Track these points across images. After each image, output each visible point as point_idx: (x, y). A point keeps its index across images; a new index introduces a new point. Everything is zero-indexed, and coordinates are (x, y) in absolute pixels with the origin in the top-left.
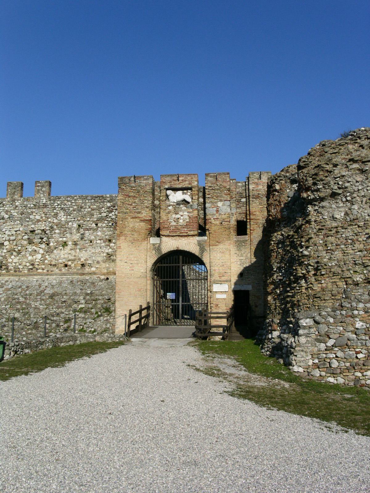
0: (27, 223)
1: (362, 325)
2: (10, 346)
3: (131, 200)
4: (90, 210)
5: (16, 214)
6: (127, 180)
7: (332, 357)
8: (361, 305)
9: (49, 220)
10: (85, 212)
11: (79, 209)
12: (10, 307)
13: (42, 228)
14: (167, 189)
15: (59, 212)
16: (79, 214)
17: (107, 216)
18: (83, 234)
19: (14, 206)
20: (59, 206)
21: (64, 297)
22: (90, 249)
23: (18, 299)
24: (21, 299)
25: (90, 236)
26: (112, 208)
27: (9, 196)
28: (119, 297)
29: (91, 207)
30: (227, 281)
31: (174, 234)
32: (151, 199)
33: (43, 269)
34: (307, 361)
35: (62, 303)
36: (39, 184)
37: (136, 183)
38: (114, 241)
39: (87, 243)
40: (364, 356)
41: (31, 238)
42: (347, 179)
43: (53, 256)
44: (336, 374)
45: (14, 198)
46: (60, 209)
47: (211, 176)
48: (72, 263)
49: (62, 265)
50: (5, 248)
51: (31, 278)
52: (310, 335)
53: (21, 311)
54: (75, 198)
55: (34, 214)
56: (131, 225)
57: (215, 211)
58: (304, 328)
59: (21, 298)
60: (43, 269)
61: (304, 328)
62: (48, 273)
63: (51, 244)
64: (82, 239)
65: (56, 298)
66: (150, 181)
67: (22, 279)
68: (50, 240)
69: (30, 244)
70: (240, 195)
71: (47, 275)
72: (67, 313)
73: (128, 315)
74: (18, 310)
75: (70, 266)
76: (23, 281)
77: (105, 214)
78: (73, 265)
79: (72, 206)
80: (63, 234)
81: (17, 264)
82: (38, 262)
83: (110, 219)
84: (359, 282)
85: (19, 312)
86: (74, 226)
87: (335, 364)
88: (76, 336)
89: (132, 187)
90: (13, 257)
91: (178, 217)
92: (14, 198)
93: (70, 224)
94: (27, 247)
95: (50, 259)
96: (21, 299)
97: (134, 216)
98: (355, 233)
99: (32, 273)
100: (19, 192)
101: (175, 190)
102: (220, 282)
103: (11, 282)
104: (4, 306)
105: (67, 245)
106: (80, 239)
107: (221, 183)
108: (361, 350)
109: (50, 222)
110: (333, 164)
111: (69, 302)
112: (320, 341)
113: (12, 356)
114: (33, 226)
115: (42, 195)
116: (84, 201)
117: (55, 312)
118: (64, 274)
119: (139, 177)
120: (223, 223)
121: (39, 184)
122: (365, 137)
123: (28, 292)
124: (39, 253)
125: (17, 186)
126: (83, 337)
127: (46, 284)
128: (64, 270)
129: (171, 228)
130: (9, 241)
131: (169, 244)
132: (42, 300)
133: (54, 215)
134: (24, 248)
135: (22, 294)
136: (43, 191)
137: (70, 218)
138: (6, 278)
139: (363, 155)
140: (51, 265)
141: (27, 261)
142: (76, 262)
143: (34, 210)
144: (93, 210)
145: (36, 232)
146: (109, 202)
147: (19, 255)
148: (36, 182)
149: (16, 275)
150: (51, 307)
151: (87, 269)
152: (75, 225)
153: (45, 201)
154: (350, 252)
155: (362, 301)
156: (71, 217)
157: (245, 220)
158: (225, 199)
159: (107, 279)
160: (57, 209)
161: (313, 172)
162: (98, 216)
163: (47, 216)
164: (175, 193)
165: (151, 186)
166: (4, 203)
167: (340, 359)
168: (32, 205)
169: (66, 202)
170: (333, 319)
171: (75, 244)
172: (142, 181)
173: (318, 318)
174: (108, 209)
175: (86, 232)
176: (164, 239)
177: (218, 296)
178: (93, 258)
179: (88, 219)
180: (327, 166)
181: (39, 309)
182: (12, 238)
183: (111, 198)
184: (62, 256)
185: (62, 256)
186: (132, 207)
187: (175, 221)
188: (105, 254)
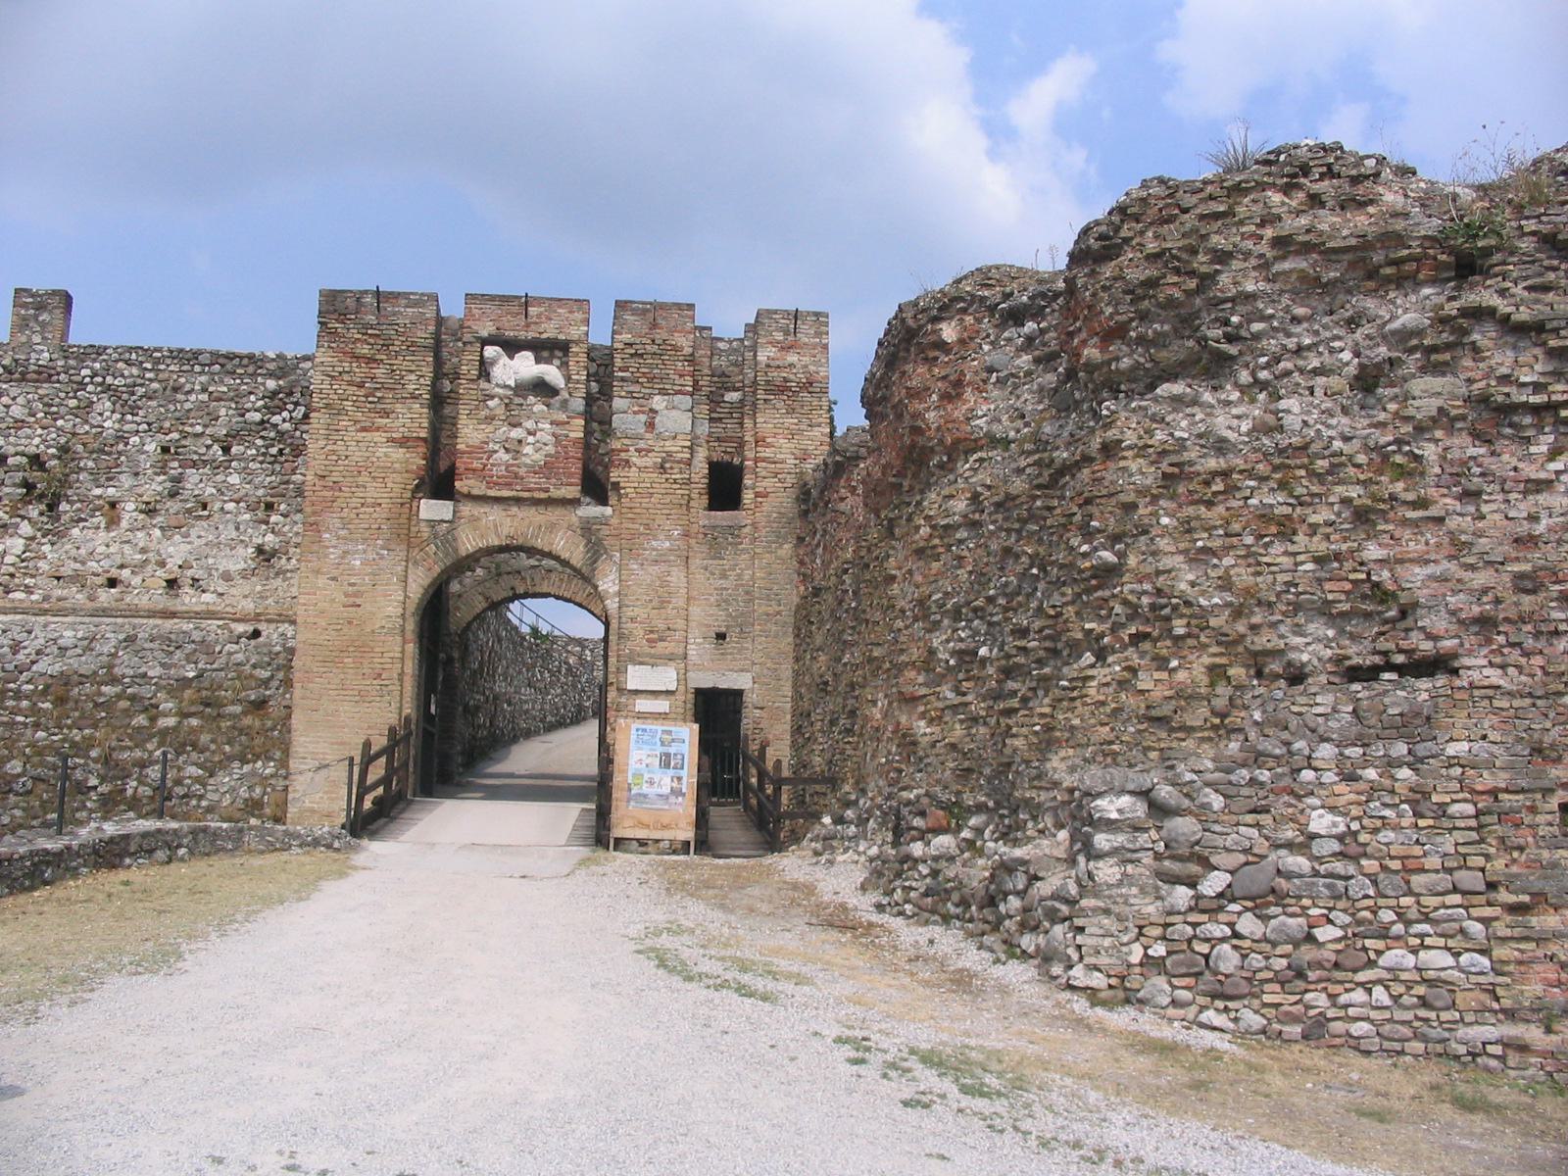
1: (1335, 825)
7: (1218, 934)
8: (1326, 751)
9: (60, 423)
11: (168, 392)
13: (32, 450)
16: (167, 411)
17: (262, 422)
20: (99, 379)
25: (201, 485)
29: (211, 389)
30: (671, 658)
32: (428, 371)
34: (1125, 949)
40: (1340, 933)
42: (1261, 306)
47: (633, 310)
52: (1138, 855)
58: (1110, 825)
61: (1110, 825)
66: (430, 313)
73: (357, 760)
77: (257, 417)
78: (136, 581)
82: (13, 565)
83: (272, 434)
84: (1307, 670)
86: (146, 448)
87: (1227, 959)
89: (368, 326)
98: (1297, 498)
101: (512, 347)
102: (652, 661)
107: (665, 336)
108: (1325, 911)
110: (1215, 251)
112: (1175, 880)
115: (37, 339)
116: (185, 368)
118: (105, 612)
120: (667, 465)
122: (1321, 170)
128: (106, 597)
131: (484, 527)
133: (78, 407)
136: (43, 325)
139: (1324, 227)
140: (58, 578)
144: (219, 399)
146: (271, 375)
151: (189, 599)
154: (1279, 560)
155: (1334, 736)
157: (736, 461)
158: (676, 388)
159: (256, 634)
160: (90, 388)
161: (1135, 275)
164: (511, 357)
165: (432, 328)
167: (1247, 944)
170: (1221, 798)
173: (1165, 792)
176: (467, 509)
178: (211, 561)
179: (199, 429)
183: (281, 364)
186: (362, 392)
187: (507, 450)
188: (251, 550)
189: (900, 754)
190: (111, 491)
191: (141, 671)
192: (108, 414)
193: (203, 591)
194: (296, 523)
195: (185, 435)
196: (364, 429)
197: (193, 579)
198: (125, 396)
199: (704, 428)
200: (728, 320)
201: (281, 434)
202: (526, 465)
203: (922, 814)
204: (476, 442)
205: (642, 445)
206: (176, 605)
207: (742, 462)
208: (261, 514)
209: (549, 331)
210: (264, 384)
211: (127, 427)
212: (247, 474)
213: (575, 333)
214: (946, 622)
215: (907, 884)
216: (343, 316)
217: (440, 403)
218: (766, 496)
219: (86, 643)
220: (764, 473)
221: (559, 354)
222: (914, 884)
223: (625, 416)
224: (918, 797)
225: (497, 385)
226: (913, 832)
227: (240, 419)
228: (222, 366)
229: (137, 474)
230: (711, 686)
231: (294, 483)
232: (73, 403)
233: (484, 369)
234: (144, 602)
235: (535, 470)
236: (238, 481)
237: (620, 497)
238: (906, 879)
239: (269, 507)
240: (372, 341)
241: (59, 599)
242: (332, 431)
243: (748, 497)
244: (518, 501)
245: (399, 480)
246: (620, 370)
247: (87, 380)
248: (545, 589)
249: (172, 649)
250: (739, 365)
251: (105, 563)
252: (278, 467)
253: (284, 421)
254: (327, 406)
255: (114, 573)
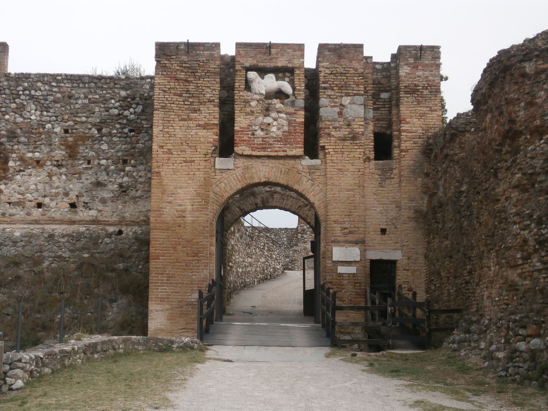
4: (86, 101)
9: (7, 117)
10: (77, 106)
14: (248, 69)
15: (25, 103)
17: (119, 114)
20: (27, 92)
25: (87, 151)
26: (129, 99)
29: (90, 96)
31: (262, 153)
38: (133, 162)
46: (28, 97)
49: (34, 204)
57: (337, 114)
70: (378, 86)
77: (116, 112)
78: (53, 204)
79: (51, 93)
83: (125, 122)
91: (269, 122)
101: (263, 72)
109: (7, 120)
116: (75, 85)
128: (37, 213)
129: (256, 142)
133: (17, 108)
137: (47, 116)
140: (9, 203)
146: (123, 88)
156: (49, 114)
157: (388, 132)
158: (355, 92)
159: (120, 232)
160: (23, 97)
162: (103, 114)
164: (263, 78)
172: (201, 52)
174: (121, 102)
177: (341, 269)
179: (84, 119)
186: (181, 99)
187: (262, 130)
188: (116, 186)
189: (508, 295)
190: (37, 154)
191: (58, 254)
192: (33, 111)
193: (90, 209)
194: (140, 171)
195: (76, 123)
196: (184, 120)
197: (84, 203)
198: (42, 101)
199: (371, 114)
200: (380, 52)
201: (129, 121)
202: (273, 137)
203: (524, 327)
204: (246, 126)
205: (337, 124)
206: (77, 218)
207: (391, 132)
208: (120, 166)
209: (281, 62)
210: (119, 93)
211: (44, 119)
212: (111, 144)
213: (296, 63)
214: (533, 225)
215: (516, 364)
216: (169, 57)
217: (227, 106)
218: (407, 152)
219: (26, 239)
220: (405, 139)
221: (288, 74)
222: (521, 365)
223: (327, 110)
224: (522, 318)
225: (256, 93)
226: (519, 337)
227: (107, 113)
228: (95, 83)
229: (51, 145)
230: (379, 258)
231: (138, 148)
232: (14, 106)
233: (248, 86)
234: (57, 216)
235: (278, 140)
236: (107, 148)
237: (325, 154)
238: (515, 362)
239: (125, 162)
240: (186, 70)
241: (11, 215)
242: (167, 122)
243: (396, 152)
244: (269, 157)
245: (203, 147)
246: (323, 83)
247: (21, 92)
248: (274, 204)
249: (74, 242)
250: (388, 77)
251: (35, 195)
252: (128, 140)
253: (131, 114)
254: (163, 107)
255: (40, 200)
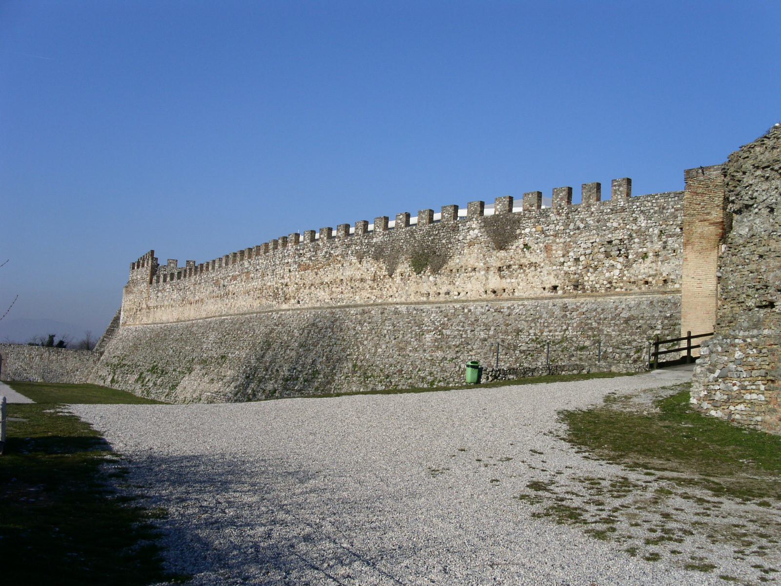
0: (604, 232)
2: (488, 370)
3: (699, 198)
5: (591, 222)
6: (694, 173)
9: (628, 227)
10: (667, 214)
12: (581, 334)
13: (620, 238)
18: (665, 242)
19: (590, 213)
20: (639, 209)
21: (640, 321)
22: (673, 261)
23: (591, 324)
24: (595, 325)
27: (584, 200)
28: (684, 322)
29: (675, 207)
33: (621, 288)
35: (637, 329)
36: (616, 183)
37: (705, 175)
39: (669, 254)
41: (608, 250)
43: (632, 271)
44: (717, 407)
45: (589, 202)
48: (653, 279)
49: (642, 282)
50: (581, 264)
51: (608, 299)
53: (592, 339)
54: (656, 197)
55: (611, 221)
56: (699, 231)
59: (593, 323)
60: (621, 288)
62: (626, 292)
63: (630, 257)
64: (664, 248)
65: (631, 323)
67: (599, 300)
68: (629, 251)
69: (607, 257)
71: (625, 294)
72: (640, 341)
74: (588, 337)
75: (651, 282)
76: (599, 302)
78: (654, 282)
79: (652, 207)
80: (642, 244)
81: (594, 282)
85: (590, 339)
86: (655, 232)
88: (582, 365)
90: (589, 274)
92: (589, 202)
93: (651, 230)
94: (604, 262)
95: (629, 275)
96: (595, 325)
97: (702, 219)
99: (609, 293)
100: (595, 195)
103: (587, 304)
104: (575, 333)
105: (647, 257)
106: (662, 248)
109: (628, 229)
111: (644, 327)
113: (490, 380)
114: (610, 236)
115: (619, 197)
117: (627, 339)
118: (644, 293)
119: (708, 168)
121: (616, 183)
123: (602, 316)
124: (617, 268)
125: (591, 188)
126: (593, 366)
127: (623, 306)
128: (644, 288)
130: (585, 255)
132: (615, 325)
134: (600, 263)
135: (596, 318)
136: (621, 192)
138: (582, 300)
141: (604, 278)
142: (657, 278)
143: (611, 216)
145: (613, 243)
147: (596, 272)
148: (613, 181)
149: (593, 296)
150: (624, 334)
151: (670, 287)
152: (656, 231)
153: (622, 203)
156: (652, 222)
163: (626, 222)
166: (579, 209)
168: (609, 210)
169: (645, 202)
171: (657, 255)
175: (669, 239)
178: (677, 272)
179: (671, 223)
180: (738, 174)
181: (611, 336)
182: (588, 251)
184: (642, 271)
185: (642, 271)
